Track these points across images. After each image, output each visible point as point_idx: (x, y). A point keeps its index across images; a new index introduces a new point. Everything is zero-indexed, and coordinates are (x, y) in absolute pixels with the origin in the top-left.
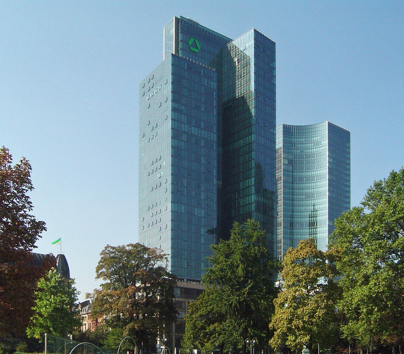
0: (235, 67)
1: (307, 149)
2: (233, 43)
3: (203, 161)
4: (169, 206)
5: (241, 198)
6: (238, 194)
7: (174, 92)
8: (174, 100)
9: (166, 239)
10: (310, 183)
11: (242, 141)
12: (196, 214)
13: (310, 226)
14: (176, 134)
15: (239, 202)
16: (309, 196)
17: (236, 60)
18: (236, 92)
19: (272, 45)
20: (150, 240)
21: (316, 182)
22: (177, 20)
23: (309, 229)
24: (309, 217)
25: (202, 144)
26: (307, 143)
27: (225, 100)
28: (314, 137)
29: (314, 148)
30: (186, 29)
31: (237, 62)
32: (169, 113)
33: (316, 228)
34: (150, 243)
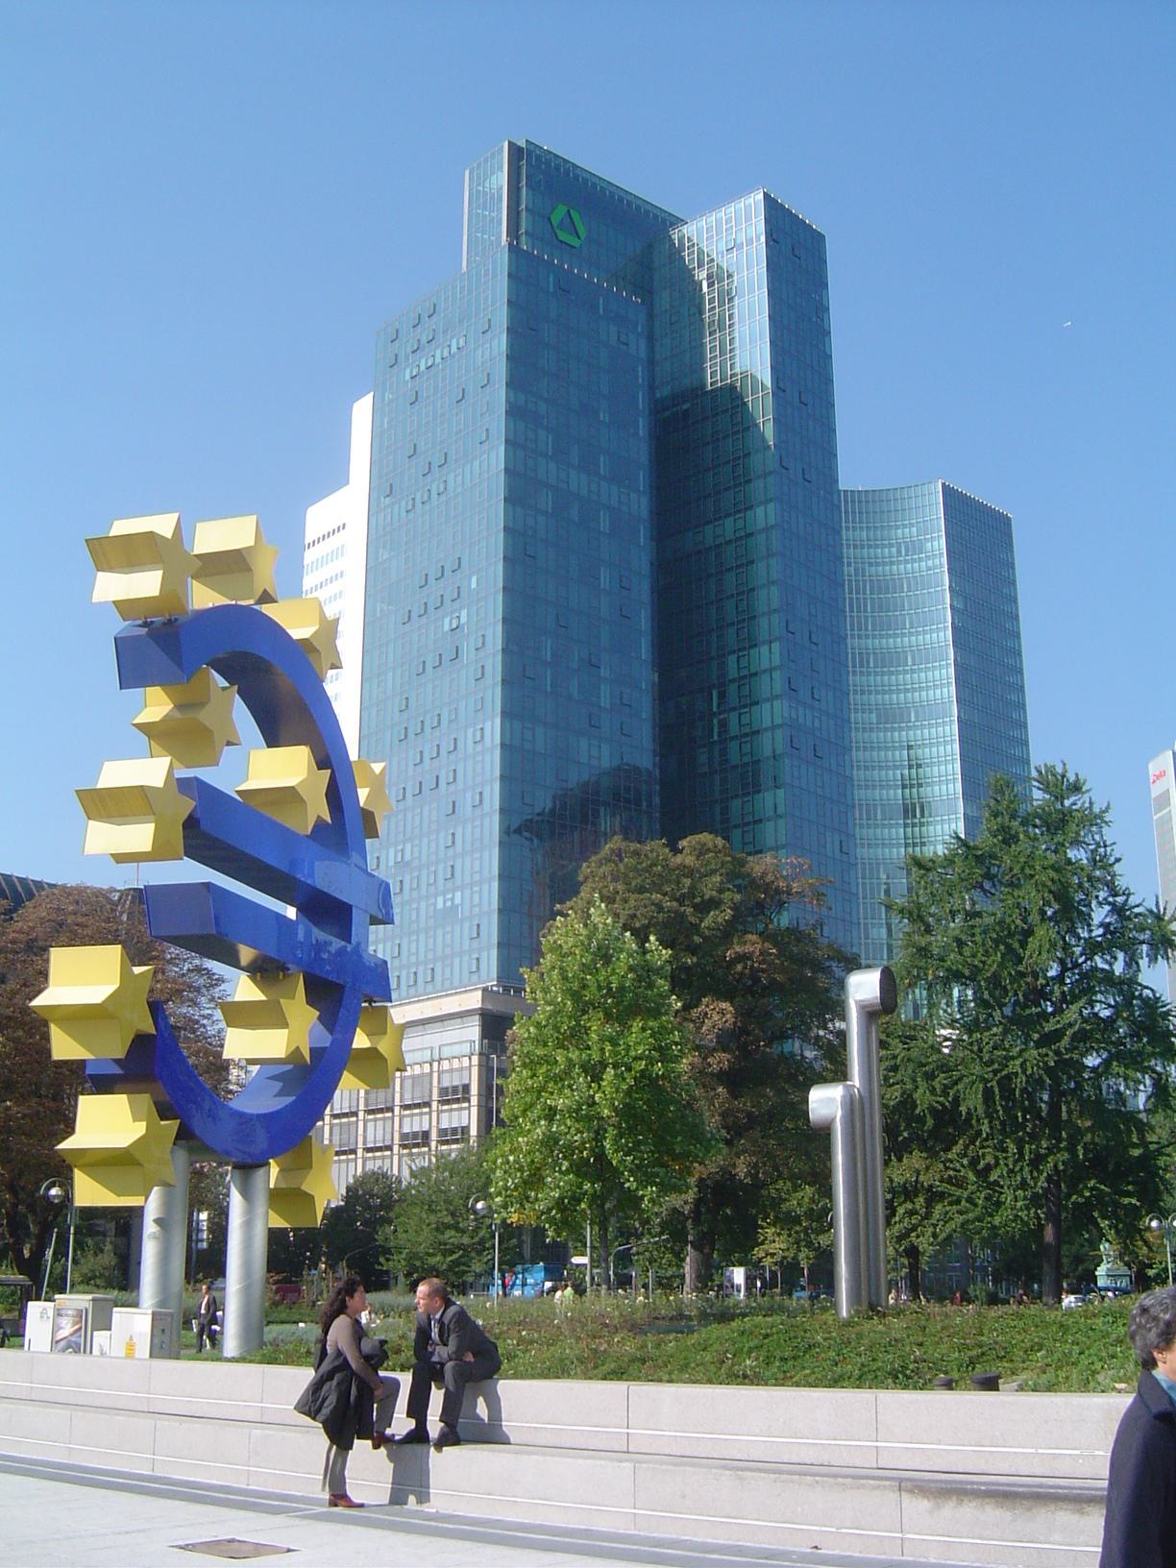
0: (702, 297)
1: (877, 564)
2: (685, 229)
3: (604, 582)
4: (493, 729)
5: (734, 709)
6: (722, 696)
7: (515, 358)
8: (515, 383)
9: (477, 844)
10: (891, 673)
11: (709, 529)
12: (584, 759)
13: (906, 817)
14: (520, 487)
15: (723, 724)
16: (892, 717)
17: (703, 275)
18: (704, 370)
19: (818, 239)
20: (408, 846)
21: (913, 671)
22: (516, 152)
23: (906, 826)
24: (904, 787)
25: (604, 524)
26: (876, 546)
27: (665, 392)
28: (897, 527)
29: (899, 563)
30: (545, 183)
31: (705, 284)
32: (497, 423)
33: (922, 825)
34: (408, 857)
